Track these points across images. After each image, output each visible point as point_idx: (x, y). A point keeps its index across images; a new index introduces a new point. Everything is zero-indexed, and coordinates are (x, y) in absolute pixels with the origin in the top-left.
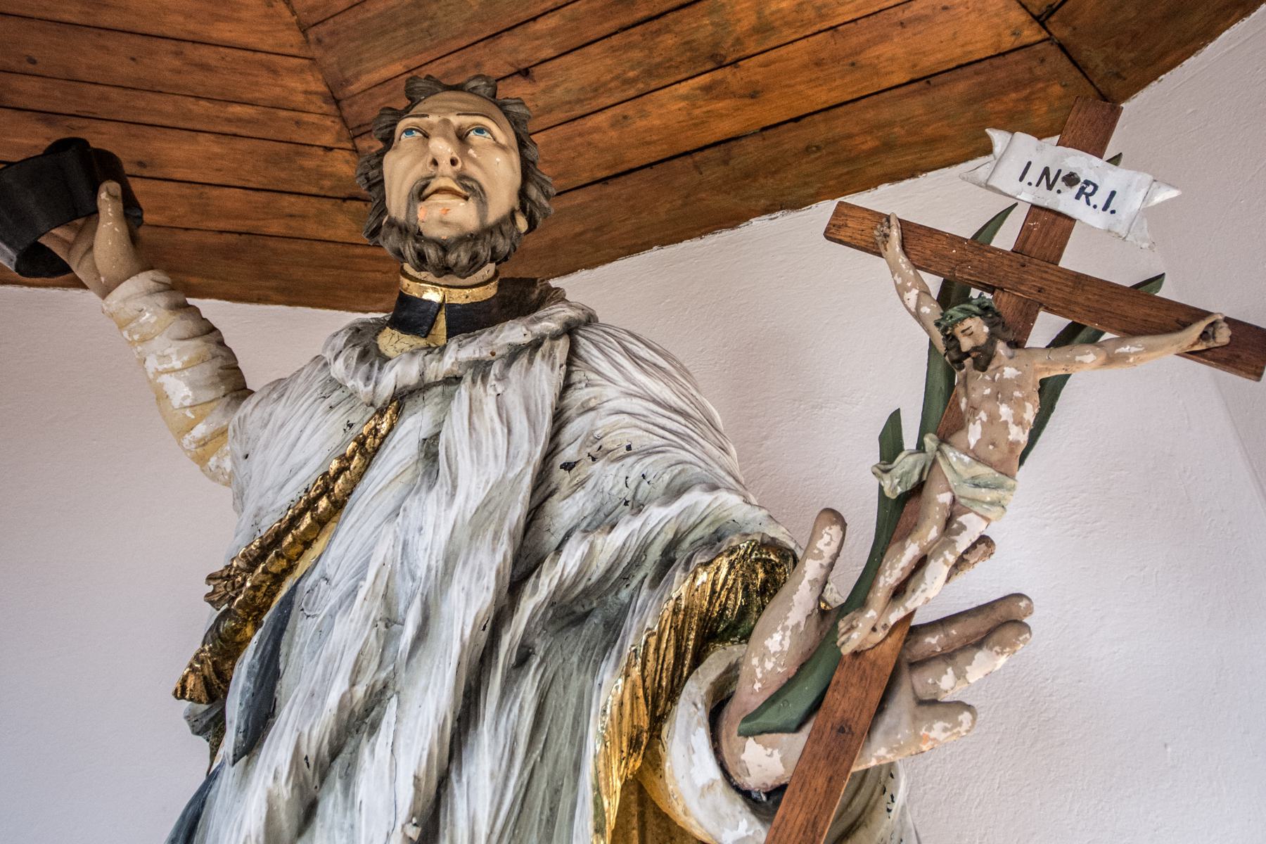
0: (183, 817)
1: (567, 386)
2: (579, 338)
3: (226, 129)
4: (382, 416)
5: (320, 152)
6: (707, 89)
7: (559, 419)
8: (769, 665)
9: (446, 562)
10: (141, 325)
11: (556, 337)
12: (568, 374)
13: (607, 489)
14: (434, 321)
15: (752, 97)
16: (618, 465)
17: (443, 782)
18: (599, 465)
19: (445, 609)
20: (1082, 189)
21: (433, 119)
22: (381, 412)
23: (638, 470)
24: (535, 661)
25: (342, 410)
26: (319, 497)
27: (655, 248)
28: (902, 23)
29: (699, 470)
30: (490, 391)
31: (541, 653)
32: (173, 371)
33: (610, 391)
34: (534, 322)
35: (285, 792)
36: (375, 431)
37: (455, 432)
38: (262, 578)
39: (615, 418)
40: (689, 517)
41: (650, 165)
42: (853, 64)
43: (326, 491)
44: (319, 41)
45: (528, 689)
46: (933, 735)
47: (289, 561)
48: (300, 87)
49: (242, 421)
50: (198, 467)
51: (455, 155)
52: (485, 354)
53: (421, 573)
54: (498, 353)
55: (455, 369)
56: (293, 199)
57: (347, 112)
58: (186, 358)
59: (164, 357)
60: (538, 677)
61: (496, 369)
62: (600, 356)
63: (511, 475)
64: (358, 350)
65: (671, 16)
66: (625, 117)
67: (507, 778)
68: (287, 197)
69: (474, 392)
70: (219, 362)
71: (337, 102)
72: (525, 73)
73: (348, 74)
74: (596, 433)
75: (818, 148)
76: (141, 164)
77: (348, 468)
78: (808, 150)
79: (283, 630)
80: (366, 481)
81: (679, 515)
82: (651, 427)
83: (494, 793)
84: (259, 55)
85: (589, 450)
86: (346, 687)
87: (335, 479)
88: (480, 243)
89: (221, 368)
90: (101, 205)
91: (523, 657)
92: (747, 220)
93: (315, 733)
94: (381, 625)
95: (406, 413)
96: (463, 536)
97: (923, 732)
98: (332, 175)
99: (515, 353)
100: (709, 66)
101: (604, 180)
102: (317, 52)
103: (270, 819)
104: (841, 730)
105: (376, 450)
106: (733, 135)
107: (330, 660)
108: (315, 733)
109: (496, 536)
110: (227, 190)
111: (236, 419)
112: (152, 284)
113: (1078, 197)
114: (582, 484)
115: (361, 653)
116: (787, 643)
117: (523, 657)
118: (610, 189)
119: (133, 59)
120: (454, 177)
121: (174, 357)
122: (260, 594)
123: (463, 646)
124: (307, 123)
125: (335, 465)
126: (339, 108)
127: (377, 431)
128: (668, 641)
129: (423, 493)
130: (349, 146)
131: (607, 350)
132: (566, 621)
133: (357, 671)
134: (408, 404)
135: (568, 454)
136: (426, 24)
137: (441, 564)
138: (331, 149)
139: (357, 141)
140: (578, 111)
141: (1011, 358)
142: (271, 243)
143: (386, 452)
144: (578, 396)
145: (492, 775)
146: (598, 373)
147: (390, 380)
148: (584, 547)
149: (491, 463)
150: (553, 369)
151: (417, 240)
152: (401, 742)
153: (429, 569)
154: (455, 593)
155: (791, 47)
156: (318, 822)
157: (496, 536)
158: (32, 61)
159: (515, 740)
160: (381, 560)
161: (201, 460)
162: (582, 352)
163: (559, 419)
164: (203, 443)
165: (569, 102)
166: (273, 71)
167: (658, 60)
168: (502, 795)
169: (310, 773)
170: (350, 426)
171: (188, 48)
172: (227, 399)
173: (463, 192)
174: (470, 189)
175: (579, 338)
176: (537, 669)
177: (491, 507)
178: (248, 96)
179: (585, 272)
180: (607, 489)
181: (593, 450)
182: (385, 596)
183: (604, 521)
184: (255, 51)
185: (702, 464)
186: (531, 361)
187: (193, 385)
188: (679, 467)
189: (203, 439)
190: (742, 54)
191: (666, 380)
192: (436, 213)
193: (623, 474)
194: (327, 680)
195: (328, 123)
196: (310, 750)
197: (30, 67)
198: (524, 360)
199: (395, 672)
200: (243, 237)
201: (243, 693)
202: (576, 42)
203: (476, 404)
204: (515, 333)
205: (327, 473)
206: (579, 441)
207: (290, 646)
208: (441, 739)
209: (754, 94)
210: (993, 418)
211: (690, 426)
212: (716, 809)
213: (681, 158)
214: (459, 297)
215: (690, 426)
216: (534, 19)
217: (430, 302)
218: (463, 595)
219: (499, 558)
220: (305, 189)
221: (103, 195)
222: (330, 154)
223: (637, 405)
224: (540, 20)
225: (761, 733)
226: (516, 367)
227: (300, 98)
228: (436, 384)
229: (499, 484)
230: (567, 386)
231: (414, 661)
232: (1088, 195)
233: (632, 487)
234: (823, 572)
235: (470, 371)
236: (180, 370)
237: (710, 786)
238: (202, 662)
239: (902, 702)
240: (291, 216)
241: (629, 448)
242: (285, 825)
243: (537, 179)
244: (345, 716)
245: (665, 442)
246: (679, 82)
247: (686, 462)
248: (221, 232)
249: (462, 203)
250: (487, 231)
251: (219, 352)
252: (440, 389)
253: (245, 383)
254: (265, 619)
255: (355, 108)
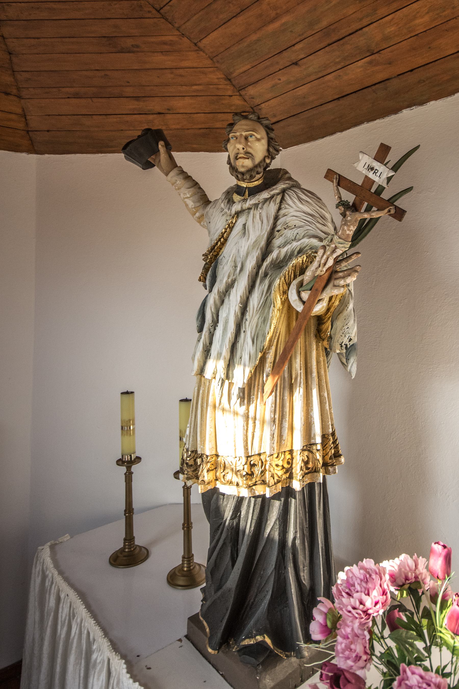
0: (202, 303)
1: (280, 209)
2: (286, 195)
3: (194, 94)
4: (233, 218)
5: (228, 97)
6: (370, 63)
7: (276, 218)
8: (307, 278)
9: (247, 255)
10: (177, 185)
11: (278, 194)
12: (280, 205)
13: (288, 237)
14: (245, 192)
15: (390, 64)
16: (291, 230)
17: (248, 298)
18: (286, 230)
19: (246, 264)
20: (375, 171)
21: (238, 134)
22: (233, 217)
23: (296, 232)
24: (269, 276)
25: (225, 216)
26: (221, 238)
27: (365, 123)
28: (446, 30)
29: (312, 232)
30: (258, 212)
31: (270, 274)
32: (187, 198)
33: (291, 210)
34: (271, 191)
35: (217, 297)
36: (232, 222)
37: (250, 223)
38: (212, 256)
39: (292, 218)
40: (303, 245)
41: (355, 92)
42: (430, 48)
43: (223, 236)
44: (218, 62)
45: (267, 282)
46: (334, 292)
47: (217, 252)
48: (215, 77)
49: (207, 212)
50: (199, 224)
51: (243, 147)
52: (257, 202)
53: (241, 256)
54: (261, 201)
55: (249, 206)
56: (222, 115)
57: (234, 83)
58: (190, 194)
59: (185, 194)
60: (269, 279)
61: (260, 206)
62: (290, 200)
63: (262, 234)
64: (227, 200)
65: (347, 38)
66: (339, 76)
67: (261, 298)
68: (220, 114)
69: (254, 212)
70: (199, 194)
71: (230, 80)
72: (296, 64)
73: (231, 70)
74: (287, 222)
75: (424, 81)
76: (169, 110)
77: (226, 231)
78: (419, 82)
79: (216, 267)
80: (231, 234)
81: (300, 244)
82: (301, 220)
83: (258, 300)
84: (198, 69)
85: (284, 227)
86: (227, 279)
87: (224, 234)
88: (253, 171)
89: (201, 196)
90: (160, 149)
91: (266, 275)
92: (401, 110)
93: (222, 287)
94: (234, 267)
95: (239, 218)
96: (251, 248)
97: (332, 291)
98: (234, 105)
99: (266, 200)
100: (368, 54)
101: (338, 99)
102: (217, 65)
103: (215, 302)
104: (316, 290)
105: (233, 227)
106: (386, 78)
107: (224, 274)
108: (222, 287)
109: (258, 248)
110: (199, 115)
111: (205, 212)
112: (178, 171)
113: (373, 174)
114: (281, 236)
115: (230, 273)
116: (310, 274)
117: (266, 275)
118: (342, 101)
119: (158, 77)
120: (244, 153)
121: (187, 194)
122: (212, 260)
123: (249, 272)
124: (221, 88)
125: (224, 230)
126: (231, 82)
127: (232, 222)
128: (291, 273)
129: (242, 238)
130: (238, 94)
131: (292, 198)
132: (278, 267)
133: (229, 276)
134: (240, 215)
135: (278, 228)
136: (254, 52)
137: (246, 255)
138: (232, 96)
139: (240, 92)
140: (321, 75)
141: (350, 215)
142: (218, 131)
143: (235, 227)
144: (282, 212)
145: (258, 297)
146: (289, 205)
147: (236, 207)
148: (278, 252)
149: (257, 232)
150: (275, 205)
151: (236, 172)
152: (238, 290)
153: (243, 256)
154: (248, 261)
155: (400, 44)
156: (224, 303)
157: (258, 248)
158: (128, 82)
159: (263, 291)
160: (233, 254)
161: (200, 222)
162: (285, 198)
163: (276, 218)
164: (199, 218)
165: (316, 72)
166: (204, 73)
167: (346, 54)
168: (260, 301)
169: (222, 294)
170: (227, 220)
171: (175, 71)
172: (203, 205)
173: (247, 157)
174: (249, 155)
175: (286, 195)
176: (269, 278)
177: (257, 242)
178: (198, 83)
179: (339, 133)
180: (288, 237)
181: (285, 226)
182: (234, 261)
183: (284, 245)
184: (197, 68)
185: (314, 230)
186: (270, 203)
187: (194, 202)
188: (307, 231)
189: (199, 217)
190: (381, 49)
191: (308, 206)
192: (241, 164)
193: (292, 233)
194: (223, 278)
195: (228, 87)
196: (221, 290)
197: (128, 84)
198: (268, 203)
199: (236, 276)
200: (208, 130)
201: (209, 280)
202: (312, 51)
203: (255, 215)
204: (265, 195)
205: (222, 232)
206: (281, 224)
207: (218, 271)
208: (246, 290)
209: (390, 63)
210: (343, 229)
211: (313, 219)
212: (296, 304)
213: (367, 89)
214: (251, 185)
215: (313, 219)
216: (294, 45)
217: (243, 187)
218: (249, 262)
219: (257, 254)
220: (226, 111)
221: (160, 146)
222: (232, 98)
223: (298, 214)
224: (296, 45)
225: (304, 291)
226: (266, 205)
227: (216, 81)
228: (246, 210)
229: (259, 236)
230: (280, 209)
231: (240, 275)
232: (376, 173)
233: (295, 236)
234: (320, 259)
235: (254, 206)
236: (190, 197)
237: (296, 300)
238: (203, 274)
239: (331, 285)
240: (223, 121)
241: (295, 226)
242: (218, 303)
243: (273, 145)
244: (228, 284)
245: (305, 224)
246: (358, 61)
247: (309, 230)
248: (200, 129)
249: (247, 160)
250: (256, 166)
251: (200, 191)
252: (247, 211)
253: (208, 199)
254: (212, 265)
255: (237, 81)
